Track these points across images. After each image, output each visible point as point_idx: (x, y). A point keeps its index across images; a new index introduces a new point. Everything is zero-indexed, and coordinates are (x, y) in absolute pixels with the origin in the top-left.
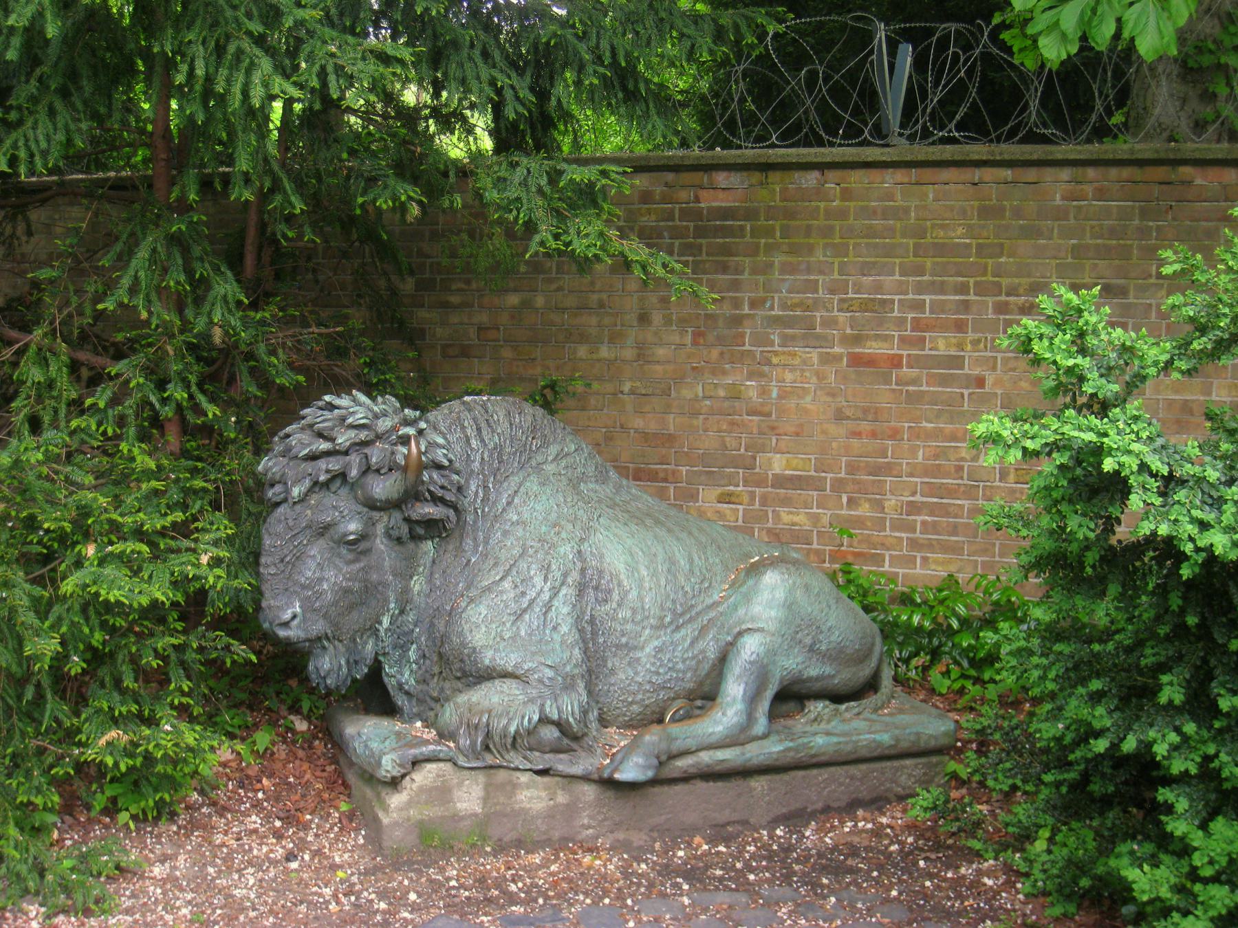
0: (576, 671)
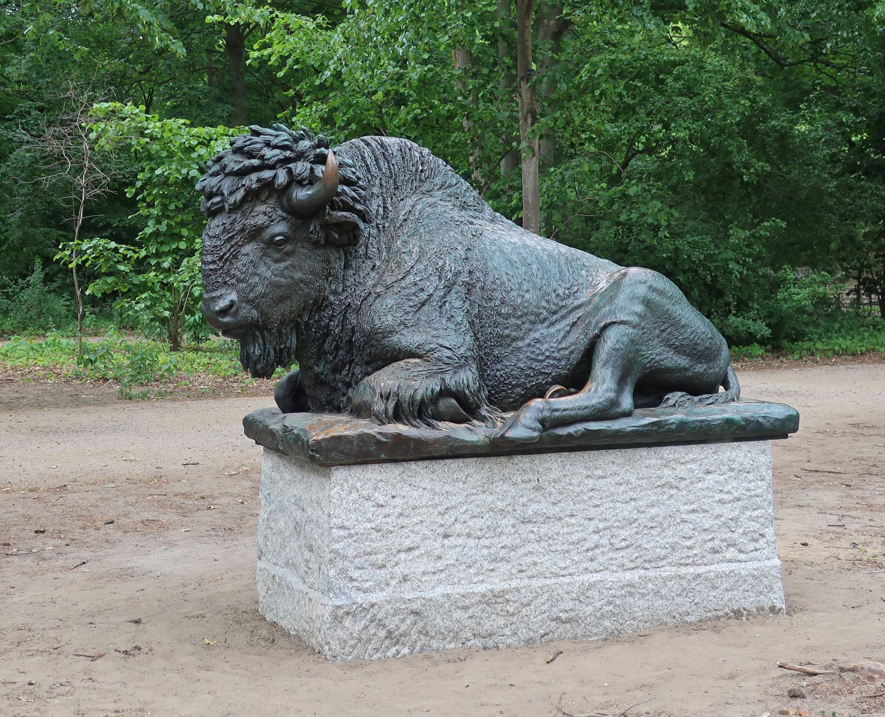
0: (469, 354)
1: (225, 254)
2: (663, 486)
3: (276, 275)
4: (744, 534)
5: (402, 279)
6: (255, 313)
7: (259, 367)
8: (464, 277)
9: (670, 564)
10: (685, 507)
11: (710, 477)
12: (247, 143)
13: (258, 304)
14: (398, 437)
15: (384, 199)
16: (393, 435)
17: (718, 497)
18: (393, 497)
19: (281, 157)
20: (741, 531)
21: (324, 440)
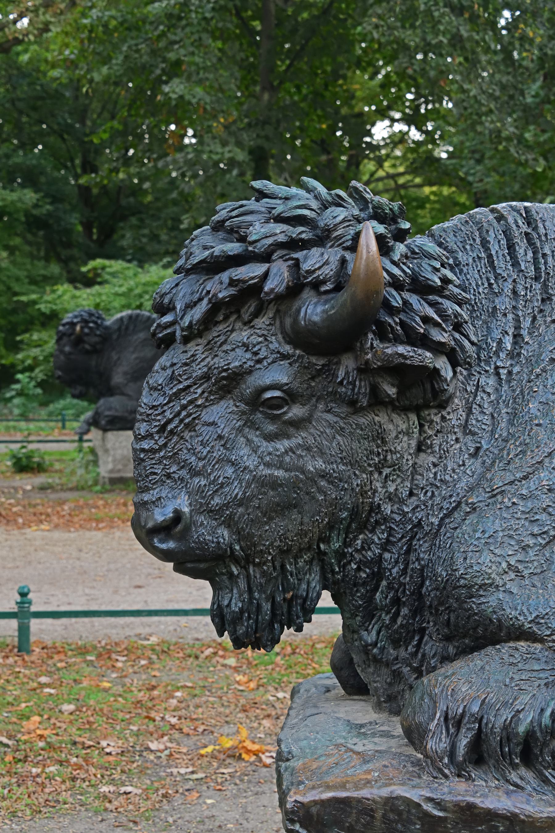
1: (169, 421)
3: (268, 465)
5: (525, 478)
7: (241, 630)
12: (234, 213)
13: (231, 517)
14: (469, 813)
15: (517, 320)
16: (457, 805)
19: (281, 238)
21: (315, 802)
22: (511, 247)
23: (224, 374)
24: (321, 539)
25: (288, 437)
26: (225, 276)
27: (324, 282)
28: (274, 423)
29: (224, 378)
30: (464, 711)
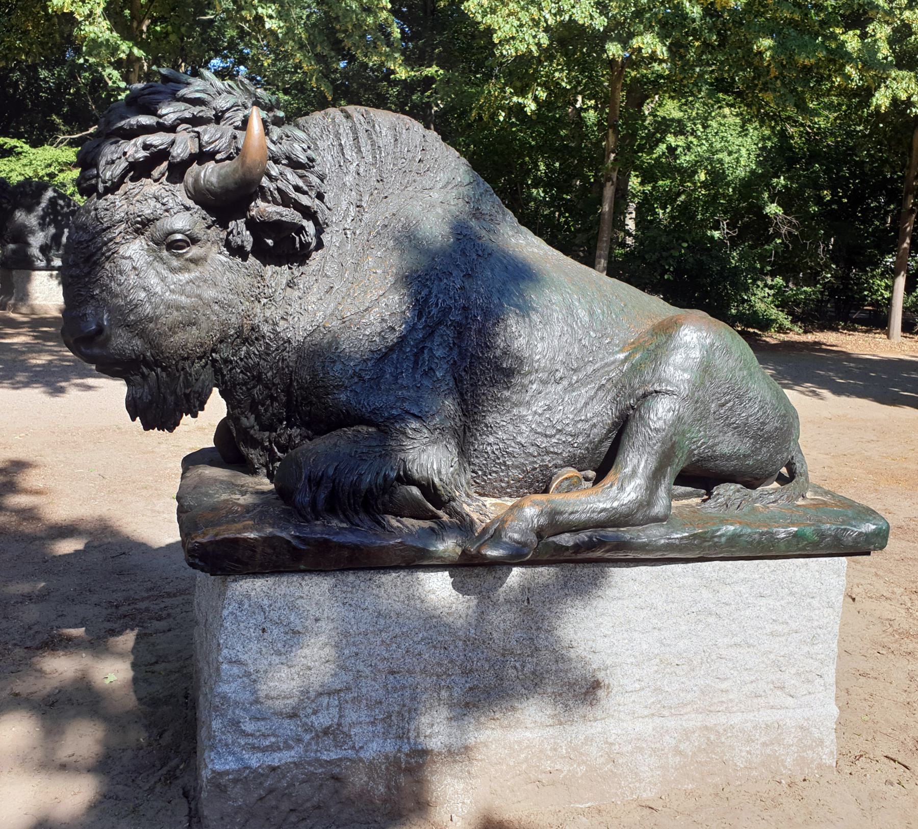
2: (699, 612)
3: (173, 292)
4: (798, 674)
6: (137, 343)
8: (455, 316)
9: (697, 711)
10: (725, 640)
11: (763, 601)
17: (769, 628)
18: (317, 620)
20: (793, 671)
22: (356, 138)
23: (139, 219)
24: (213, 351)
25: (189, 271)
26: (140, 140)
27: (218, 152)
28: (178, 260)
29: (138, 222)
30: (323, 474)
